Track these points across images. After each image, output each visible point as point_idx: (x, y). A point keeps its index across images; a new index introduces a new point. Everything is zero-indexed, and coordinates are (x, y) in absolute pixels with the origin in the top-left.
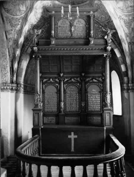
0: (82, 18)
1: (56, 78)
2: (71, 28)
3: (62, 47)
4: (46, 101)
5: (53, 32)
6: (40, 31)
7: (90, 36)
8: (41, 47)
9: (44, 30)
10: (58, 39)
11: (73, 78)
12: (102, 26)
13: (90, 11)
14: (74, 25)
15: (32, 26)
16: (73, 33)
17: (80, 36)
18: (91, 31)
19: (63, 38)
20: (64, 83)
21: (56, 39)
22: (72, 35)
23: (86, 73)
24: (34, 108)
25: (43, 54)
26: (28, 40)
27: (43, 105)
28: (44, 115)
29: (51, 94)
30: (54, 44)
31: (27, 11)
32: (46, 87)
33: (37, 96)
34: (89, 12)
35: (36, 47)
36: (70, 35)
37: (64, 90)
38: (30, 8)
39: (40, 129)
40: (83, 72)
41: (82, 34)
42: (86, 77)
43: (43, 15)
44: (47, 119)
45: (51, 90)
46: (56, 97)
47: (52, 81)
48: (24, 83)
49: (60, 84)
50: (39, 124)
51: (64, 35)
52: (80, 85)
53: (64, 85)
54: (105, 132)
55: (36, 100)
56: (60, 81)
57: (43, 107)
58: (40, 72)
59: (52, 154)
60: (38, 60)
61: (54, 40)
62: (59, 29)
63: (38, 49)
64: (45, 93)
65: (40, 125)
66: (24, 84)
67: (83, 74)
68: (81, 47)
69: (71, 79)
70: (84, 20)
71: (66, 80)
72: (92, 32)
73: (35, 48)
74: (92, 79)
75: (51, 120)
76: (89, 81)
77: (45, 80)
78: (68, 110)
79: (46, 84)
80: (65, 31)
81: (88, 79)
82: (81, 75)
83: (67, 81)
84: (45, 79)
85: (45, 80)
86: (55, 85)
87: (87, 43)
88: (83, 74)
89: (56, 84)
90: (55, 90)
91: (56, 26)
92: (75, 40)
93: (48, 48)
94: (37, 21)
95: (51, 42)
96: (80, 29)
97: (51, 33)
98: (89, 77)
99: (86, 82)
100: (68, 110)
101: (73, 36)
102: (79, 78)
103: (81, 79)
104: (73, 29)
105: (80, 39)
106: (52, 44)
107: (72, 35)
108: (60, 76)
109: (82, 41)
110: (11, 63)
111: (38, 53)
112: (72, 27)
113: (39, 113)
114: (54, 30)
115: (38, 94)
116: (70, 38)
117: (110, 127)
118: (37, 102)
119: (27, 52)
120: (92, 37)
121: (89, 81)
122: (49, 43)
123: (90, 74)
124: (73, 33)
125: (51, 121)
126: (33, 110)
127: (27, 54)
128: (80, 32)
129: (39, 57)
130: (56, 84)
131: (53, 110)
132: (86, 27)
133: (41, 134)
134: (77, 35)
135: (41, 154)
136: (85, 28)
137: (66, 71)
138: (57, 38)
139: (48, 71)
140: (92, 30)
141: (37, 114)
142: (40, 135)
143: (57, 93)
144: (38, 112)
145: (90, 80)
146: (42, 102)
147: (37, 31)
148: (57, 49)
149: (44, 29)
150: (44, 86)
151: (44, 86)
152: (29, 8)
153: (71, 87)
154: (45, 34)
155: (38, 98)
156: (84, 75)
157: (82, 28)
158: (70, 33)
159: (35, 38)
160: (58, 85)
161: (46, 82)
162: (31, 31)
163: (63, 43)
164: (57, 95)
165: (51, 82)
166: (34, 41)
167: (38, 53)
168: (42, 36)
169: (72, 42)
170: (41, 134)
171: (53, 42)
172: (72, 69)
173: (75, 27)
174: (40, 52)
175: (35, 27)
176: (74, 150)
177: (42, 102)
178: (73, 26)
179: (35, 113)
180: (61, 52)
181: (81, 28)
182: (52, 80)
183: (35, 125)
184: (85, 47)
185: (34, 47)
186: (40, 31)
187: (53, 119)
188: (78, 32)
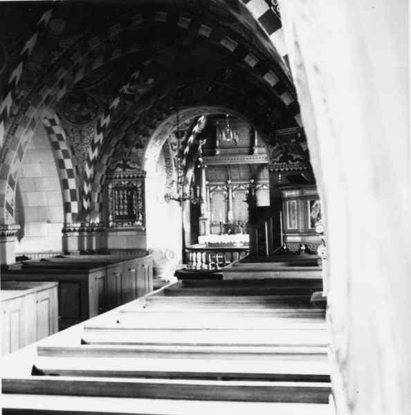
1: (223, 185)
6: (205, 140)
11: (242, 185)
12: (185, 144)
20: (233, 191)
21: (221, 148)
25: (208, 164)
45: (220, 199)
49: (228, 191)
56: (228, 188)
58: (207, 180)
67: (252, 181)
69: (239, 186)
71: (235, 187)
73: (200, 159)
74: (262, 186)
77: (212, 188)
83: (236, 188)
85: (212, 188)
90: (224, 199)
108: (227, 183)
109: (246, 150)
110: (22, 255)
116: (234, 148)
117: (288, 226)
122: (213, 154)
137: (233, 177)
143: (225, 201)
153: (240, 195)
161: (213, 190)
165: (219, 191)
171: (218, 152)
172: (240, 175)
176: (264, 81)
184: (249, 157)
186: (205, 140)
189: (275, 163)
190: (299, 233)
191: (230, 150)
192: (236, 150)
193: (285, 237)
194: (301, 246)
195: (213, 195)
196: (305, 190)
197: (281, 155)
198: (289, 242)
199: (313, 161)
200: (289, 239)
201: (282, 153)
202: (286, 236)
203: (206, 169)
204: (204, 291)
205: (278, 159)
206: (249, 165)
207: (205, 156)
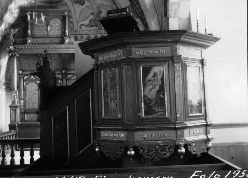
0: (58, 18)
2: (47, 27)
3: (35, 46)
4: (27, 98)
5: (29, 32)
7: (65, 36)
8: (17, 47)
9: (21, 29)
10: (35, 38)
13: (65, 12)
14: (50, 24)
15: (10, 25)
16: (49, 32)
17: (56, 35)
18: (66, 30)
19: (39, 37)
21: (33, 38)
22: (48, 34)
23: (66, 70)
24: (12, 104)
25: (19, 53)
26: (6, 38)
27: (24, 102)
28: (22, 113)
29: (33, 91)
30: (30, 43)
31: (3, 11)
32: (27, 84)
33: (14, 93)
34: (64, 12)
35: (12, 45)
36: (47, 34)
37: (24, 88)
38: (5, 10)
39: (17, 124)
40: (63, 69)
41: (58, 33)
42: (24, 74)
43: (20, 14)
44: (28, 116)
46: (38, 94)
47: (33, 78)
48: (5, 80)
50: (15, 121)
51: (40, 34)
52: (62, 82)
53: (24, 82)
54: (17, 127)
55: (13, 97)
56: (62, 77)
57: (24, 104)
59: (68, 149)
60: (15, 60)
61: (30, 39)
62: (35, 28)
63: (15, 48)
64: (26, 90)
65: (16, 121)
66: (6, 82)
67: (64, 71)
68: (57, 46)
70: (60, 19)
71: (26, 77)
72: (67, 31)
75: (33, 118)
76: (70, 78)
77: (26, 77)
78: (27, 107)
79: (27, 82)
80: (42, 30)
81: (69, 76)
82: (62, 72)
84: (26, 76)
86: (36, 81)
87: (62, 42)
88: (64, 71)
89: (37, 81)
91: (33, 25)
92: (52, 39)
93: (65, 47)
94: (14, 20)
95: (27, 42)
96: (56, 28)
97: (27, 32)
98: (70, 74)
99: (67, 79)
100: (27, 107)
101: (49, 35)
102: (60, 75)
103: (62, 76)
104: (49, 29)
105: (56, 38)
106: (66, 43)
107: (48, 34)
109: (58, 40)
111: (15, 51)
112: (49, 27)
113: (15, 110)
114: (30, 29)
115: (14, 91)
116: (46, 37)
118: (14, 99)
119: (6, 49)
120: (67, 36)
121: (70, 78)
122: (25, 42)
123: (72, 71)
124: (49, 32)
125: (32, 119)
126: (10, 107)
127: (6, 51)
128: (56, 31)
129: (15, 55)
130: (37, 81)
131: (34, 107)
132: (62, 27)
133: (17, 129)
134: (53, 34)
135: (18, 149)
136: (61, 27)
138: (33, 36)
139: (29, 69)
140: (67, 30)
141: (13, 111)
142: (16, 130)
144: (14, 108)
145: (72, 77)
146: (23, 99)
147: (14, 30)
148: (28, 48)
149: (21, 28)
150: (25, 83)
151: (25, 83)
152: (4, 9)
154: (21, 33)
155: (15, 95)
156: (65, 72)
157: (58, 27)
158: (46, 32)
159: (12, 37)
160: (61, 81)
161: (27, 79)
162: (8, 30)
163: (39, 42)
164: (38, 92)
165: (32, 80)
166: (11, 40)
167: (15, 51)
168: (19, 36)
169: (48, 40)
170: (17, 129)
173: (51, 27)
174: (16, 50)
175: (13, 26)
177: (23, 99)
178: (49, 25)
179: (12, 110)
180: (37, 50)
181: (57, 27)
182: (34, 77)
183: (12, 121)
185: (10, 45)
186: (17, 30)
187: (34, 116)
188: (54, 31)
189: (84, 28)
190: (124, 124)
191: (41, 40)
192: (48, 40)
193: (97, 132)
194: (127, 149)
195: (27, 84)
196: (124, 140)
197: (92, 17)
198: (103, 141)
199: (144, 13)
200: (105, 135)
201: (92, 13)
202: (100, 130)
203: (18, 57)
204: (229, 144)
205: (87, 22)
206: (60, 55)
207: (17, 44)
